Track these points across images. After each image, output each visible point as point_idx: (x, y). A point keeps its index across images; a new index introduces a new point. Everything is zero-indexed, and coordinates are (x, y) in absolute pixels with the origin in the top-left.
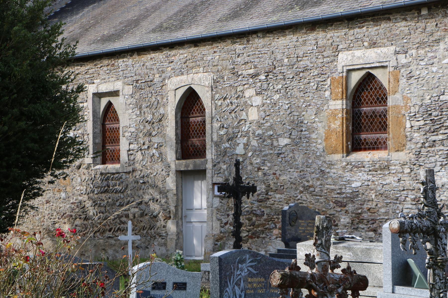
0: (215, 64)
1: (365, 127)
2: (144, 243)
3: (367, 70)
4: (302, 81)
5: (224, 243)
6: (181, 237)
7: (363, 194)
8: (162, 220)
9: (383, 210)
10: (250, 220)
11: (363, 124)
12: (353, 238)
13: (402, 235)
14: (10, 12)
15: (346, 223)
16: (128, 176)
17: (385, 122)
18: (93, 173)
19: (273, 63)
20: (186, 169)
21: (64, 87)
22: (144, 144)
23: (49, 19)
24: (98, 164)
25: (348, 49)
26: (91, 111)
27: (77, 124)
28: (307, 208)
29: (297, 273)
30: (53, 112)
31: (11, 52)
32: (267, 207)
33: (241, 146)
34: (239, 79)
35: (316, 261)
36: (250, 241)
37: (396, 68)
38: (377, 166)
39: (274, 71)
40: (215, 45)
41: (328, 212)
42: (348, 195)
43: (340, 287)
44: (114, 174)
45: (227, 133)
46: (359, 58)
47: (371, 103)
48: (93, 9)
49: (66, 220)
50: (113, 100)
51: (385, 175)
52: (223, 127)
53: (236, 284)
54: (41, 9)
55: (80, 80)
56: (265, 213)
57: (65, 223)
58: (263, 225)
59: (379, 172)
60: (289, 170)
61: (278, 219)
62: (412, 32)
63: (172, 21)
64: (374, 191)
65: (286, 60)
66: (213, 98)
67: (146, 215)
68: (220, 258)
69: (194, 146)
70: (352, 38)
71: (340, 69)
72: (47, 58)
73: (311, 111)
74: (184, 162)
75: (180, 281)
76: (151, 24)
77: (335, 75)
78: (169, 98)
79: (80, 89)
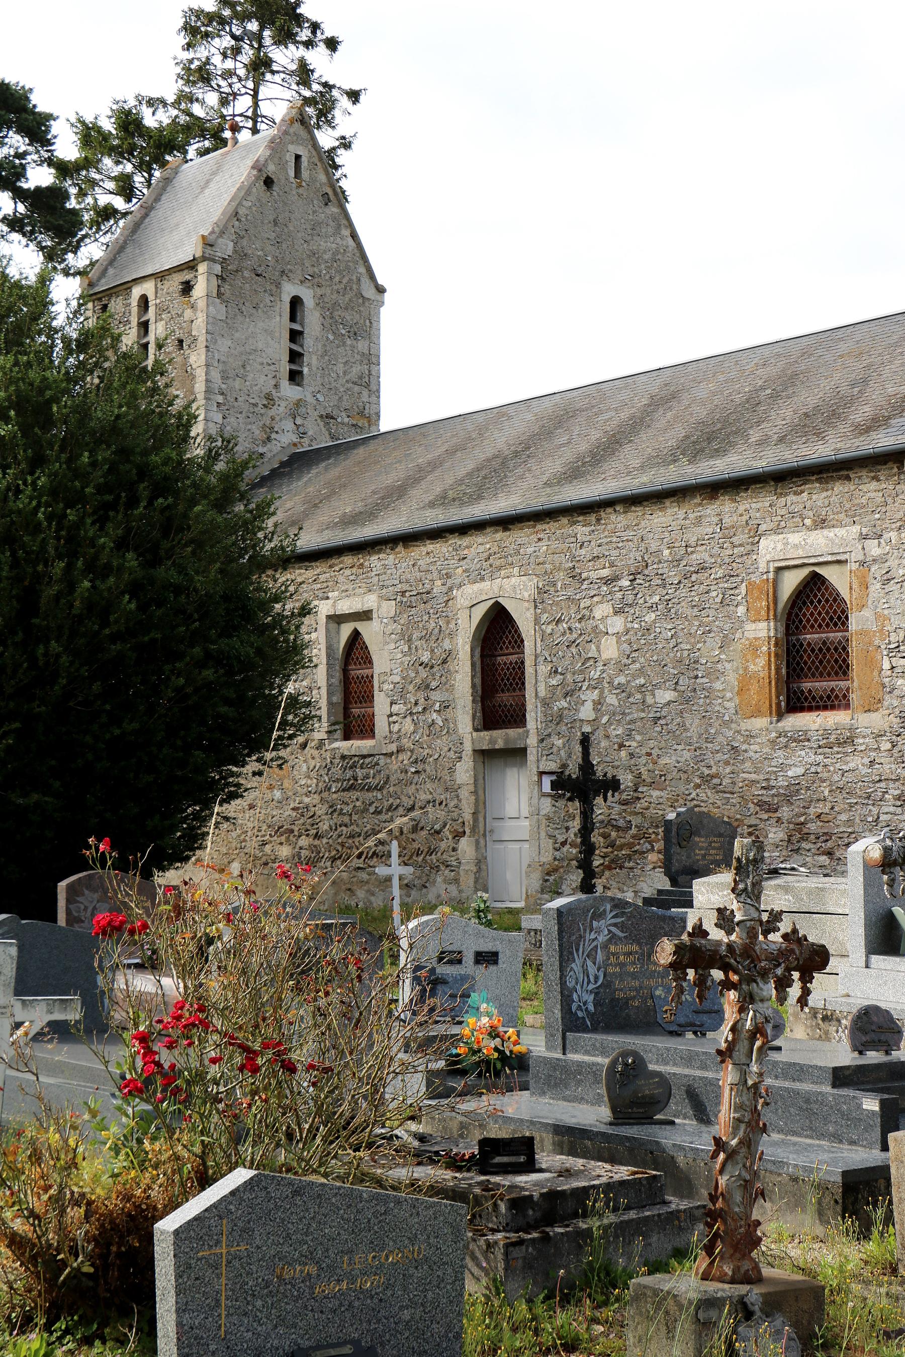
0: (541, 560)
1: (809, 669)
2: (419, 878)
3: (812, 569)
4: (696, 587)
5: (561, 878)
6: (483, 867)
7: (808, 789)
8: (450, 837)
9: (844, 817)
10: (605, 836)
11: (805, 663)
12: (793, 869)
13: (887, 870)
14: (188, 482)
15: (778, 840)
16: (389, 761)
17: (844, 661)
18: (328, 755)
19: (643, 558)
20: (490, 747)
21: (278, 606)
22: (416, 704)
23: (251, 489)
24: (336, 740)
25: (777, 530)
26: (323, 647)
27: (302, 671)
28: (708, 815)
29: (703, 942)
30: (259, 652)
31: (189, 549)
32: (637, 814)
33: (589, 705)
34: (584, 587)
35: (736, 920)
36: (607, 873)
37: (862, 563)
38: (832, 738)
39: (646, 572)
40: (539, 527)
41: (746, 822)
42: (782, 791)
43: (779, 965)
44: (364, 757)
45: (562, 684)
46: (796, 546)
47: (820, 626)
48: (326, 469)
49: (283, 839)
50: (361, 627)
51: (846, 754)
52: (556, 672)
53: (588, 956)
54: (239, 475)
55: (305, 595)
56: (634, 823)
57: (281, 844)
58: (630, 846)
59: (835, 749)
60: (676, 747)
61: (657, 834)
62: (890, 500)
63: (464, 487)
64: (828, 783)
65: (666, 552)
66: (537, 621)
67: (422, 828)
68: (559, 911)
69: (505, 706)
70: (783, 512)
71: (762, 567)
72: (250, 557)
73: (712, 644)
74: (486, 734)
75: (486, 950)
76: (426, 492)
77: (753, 578)
78: (459, 621)
79: (305, 610)
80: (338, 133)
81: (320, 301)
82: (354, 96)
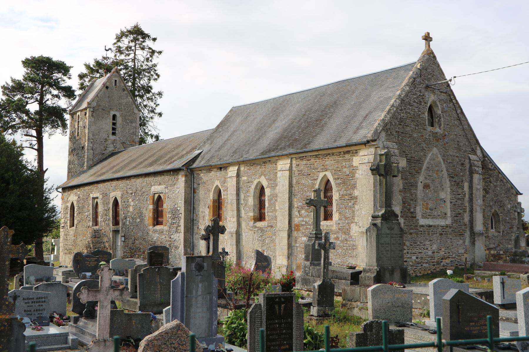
80: (153, 63)
81: (121, 115)
82: (160, 52)
